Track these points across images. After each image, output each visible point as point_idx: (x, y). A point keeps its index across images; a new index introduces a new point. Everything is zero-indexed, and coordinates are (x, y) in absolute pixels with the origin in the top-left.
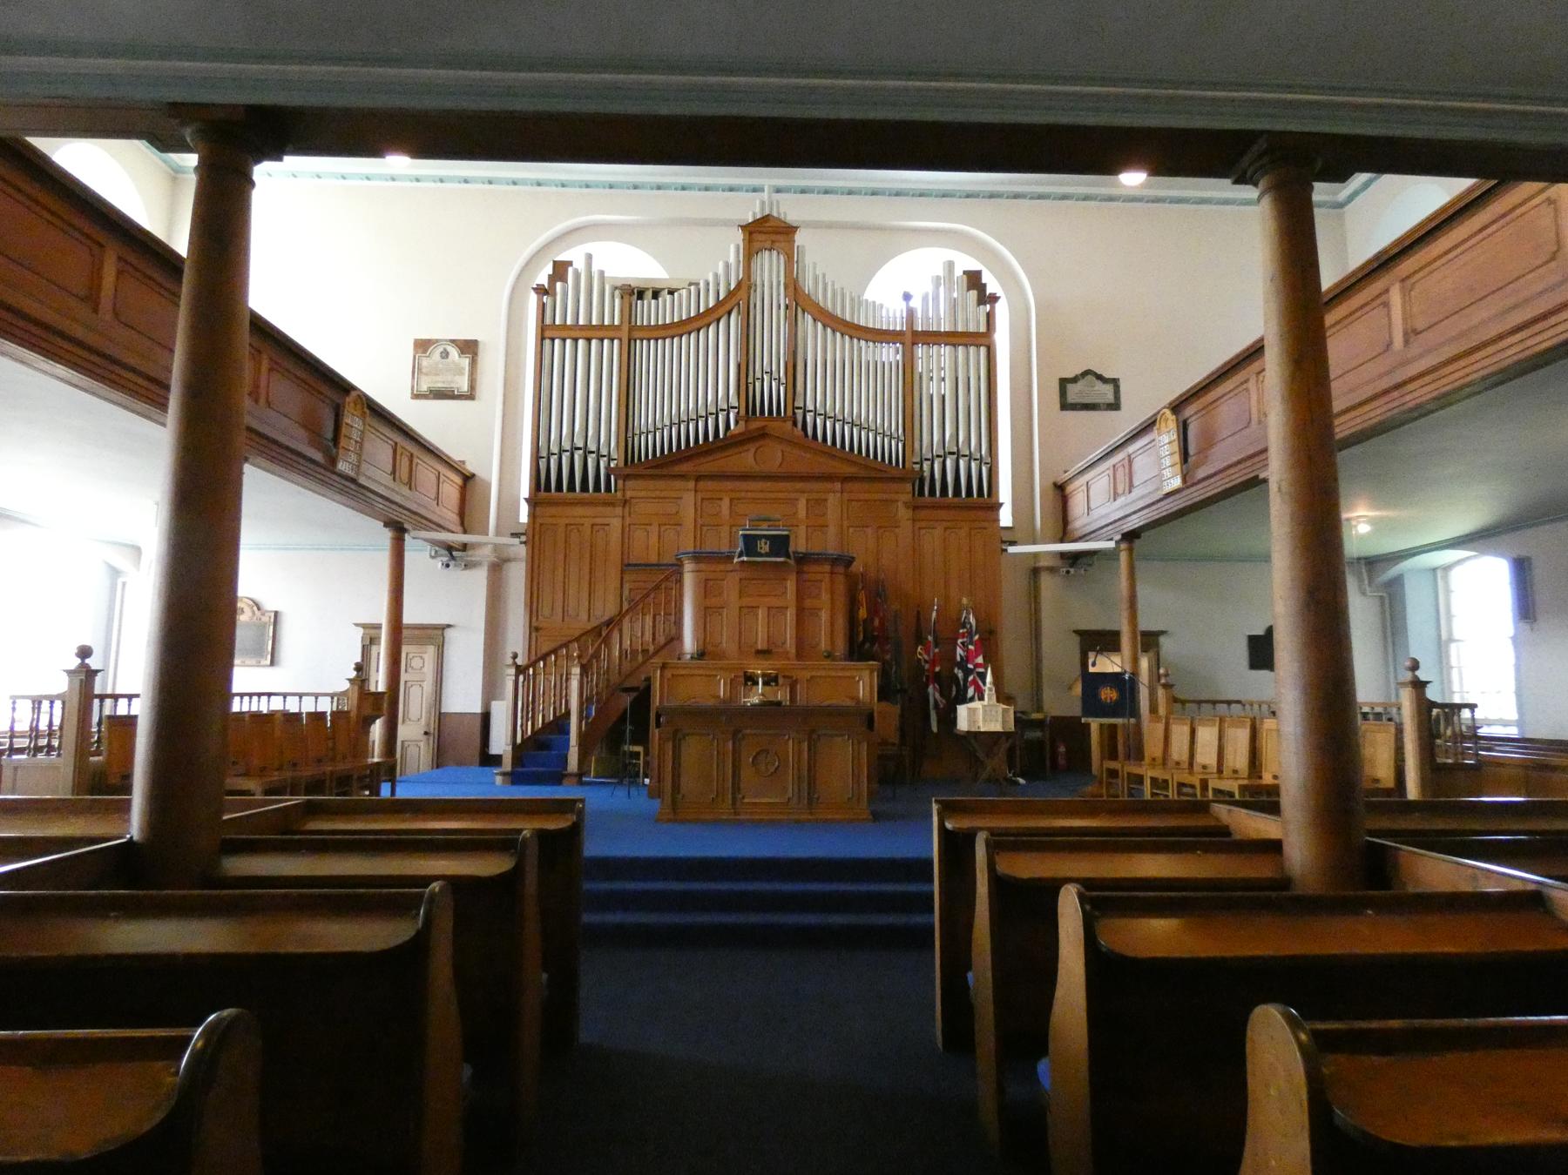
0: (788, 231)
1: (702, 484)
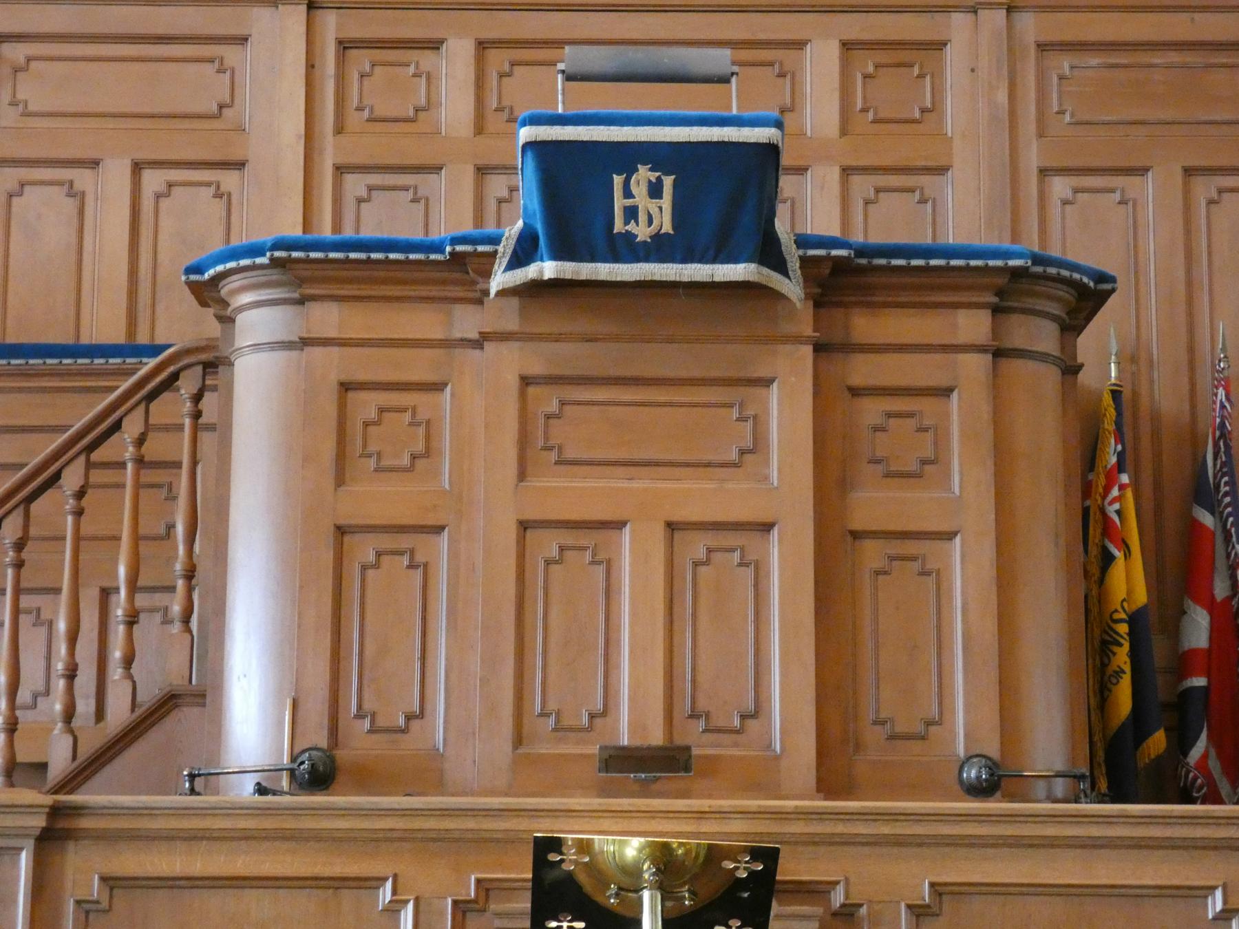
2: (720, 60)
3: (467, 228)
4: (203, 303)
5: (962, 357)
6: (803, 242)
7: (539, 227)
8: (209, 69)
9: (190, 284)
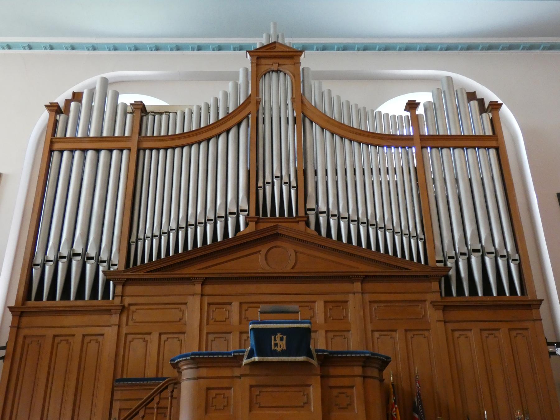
0: (292, 55)
1: (209, 289)
2: (295, 307)
3: (238, 349)
4: (174, 368)
5: (356, 378)
6: (317, 351)
7: (254, 349)
8: (177, 310)
9: (171, 364)
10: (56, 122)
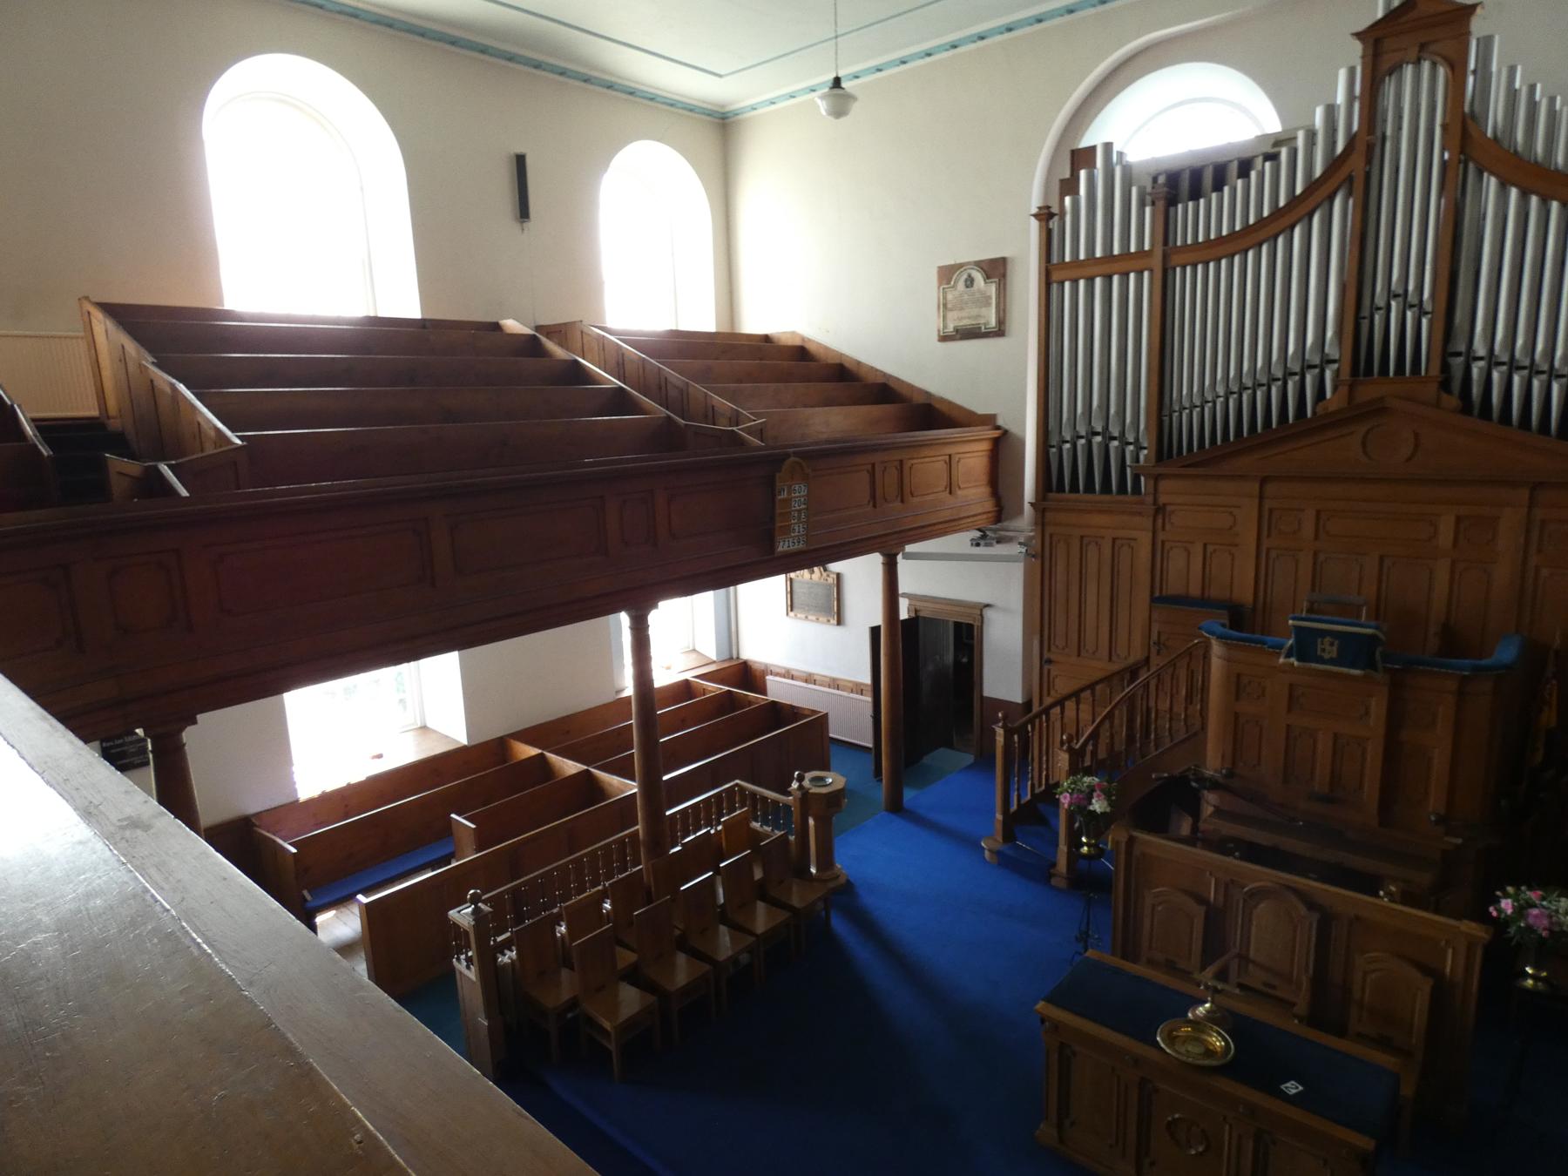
10: (1049, 232)
